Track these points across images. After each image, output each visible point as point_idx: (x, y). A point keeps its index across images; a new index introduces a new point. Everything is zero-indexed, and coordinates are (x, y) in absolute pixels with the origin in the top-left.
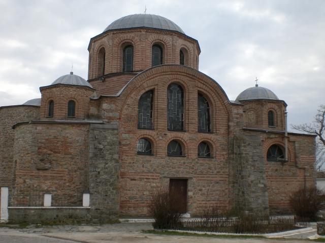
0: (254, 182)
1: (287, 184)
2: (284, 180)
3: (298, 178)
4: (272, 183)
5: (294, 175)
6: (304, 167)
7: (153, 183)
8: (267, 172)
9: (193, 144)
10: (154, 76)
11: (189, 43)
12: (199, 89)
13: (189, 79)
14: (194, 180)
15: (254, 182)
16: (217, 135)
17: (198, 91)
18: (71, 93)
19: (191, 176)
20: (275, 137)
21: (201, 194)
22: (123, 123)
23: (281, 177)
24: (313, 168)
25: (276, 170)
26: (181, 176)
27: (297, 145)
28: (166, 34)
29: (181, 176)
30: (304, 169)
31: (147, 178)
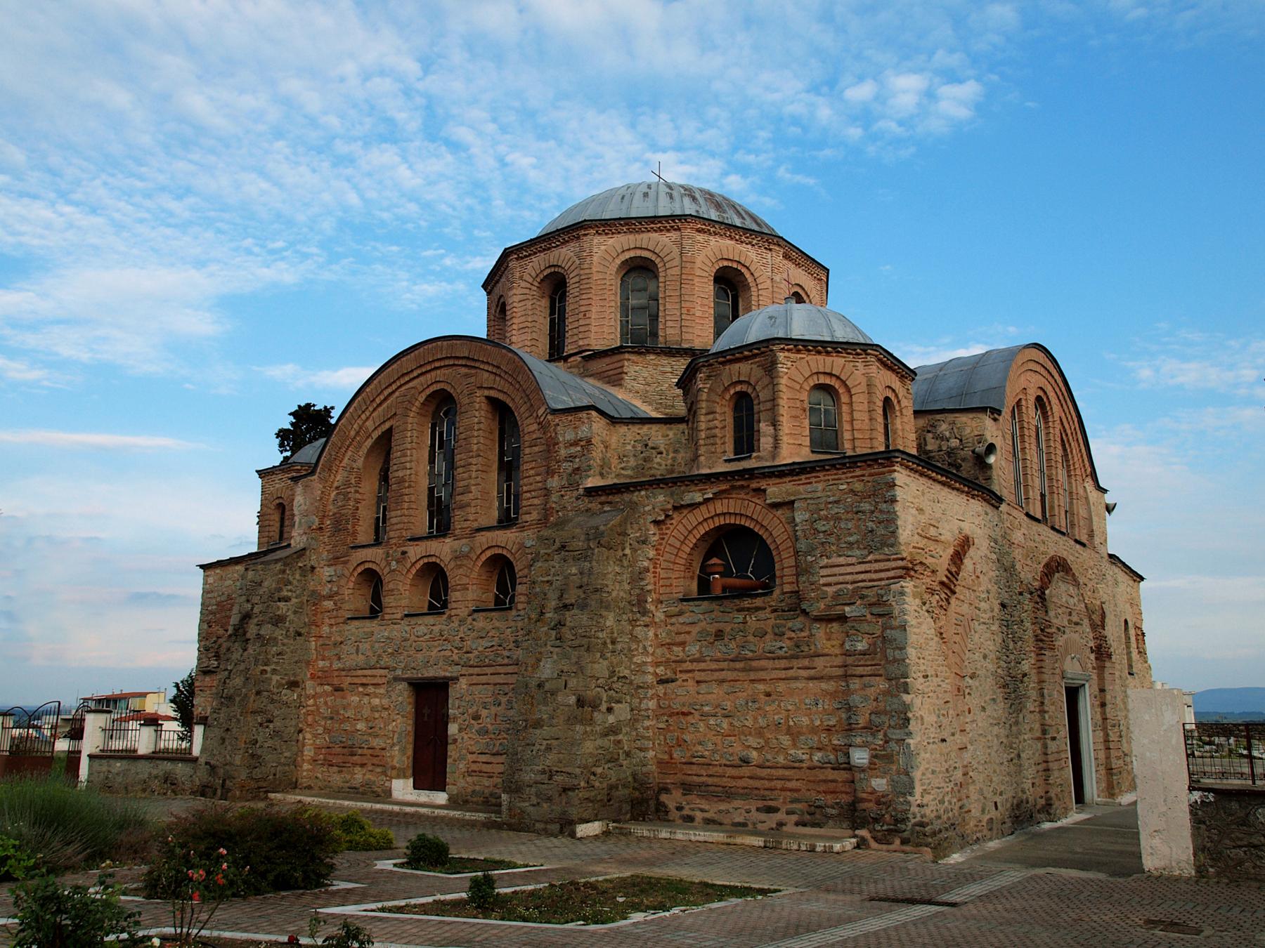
0: (547, 686)
1: (768, 695)
2: (753, 676)
3: (819, 662)
4: (703, 687)
5: (800, 651)
6: (837, 610)
7: (376, 696)
8: (683, 644)
9: (461, 571)
10: (386, 393)
11: (655, 235)
12: (487, 393)
13: (464, 370)
14: (463, 682)
15: (547, 686)
16: (522, 529)
17: (487, 397)
18: (277, 486)
19: (455, 675)
20: (707, 501)
21: (479, 732)
22: (326, 540)
23: (739, 665)
24: (888, 615)
25: (719, 635)
26: (431, 675)
27: (799, 517)
28: (565, 242)
29: (430, 673)
30: (842, 619)
31: (363, 685)
